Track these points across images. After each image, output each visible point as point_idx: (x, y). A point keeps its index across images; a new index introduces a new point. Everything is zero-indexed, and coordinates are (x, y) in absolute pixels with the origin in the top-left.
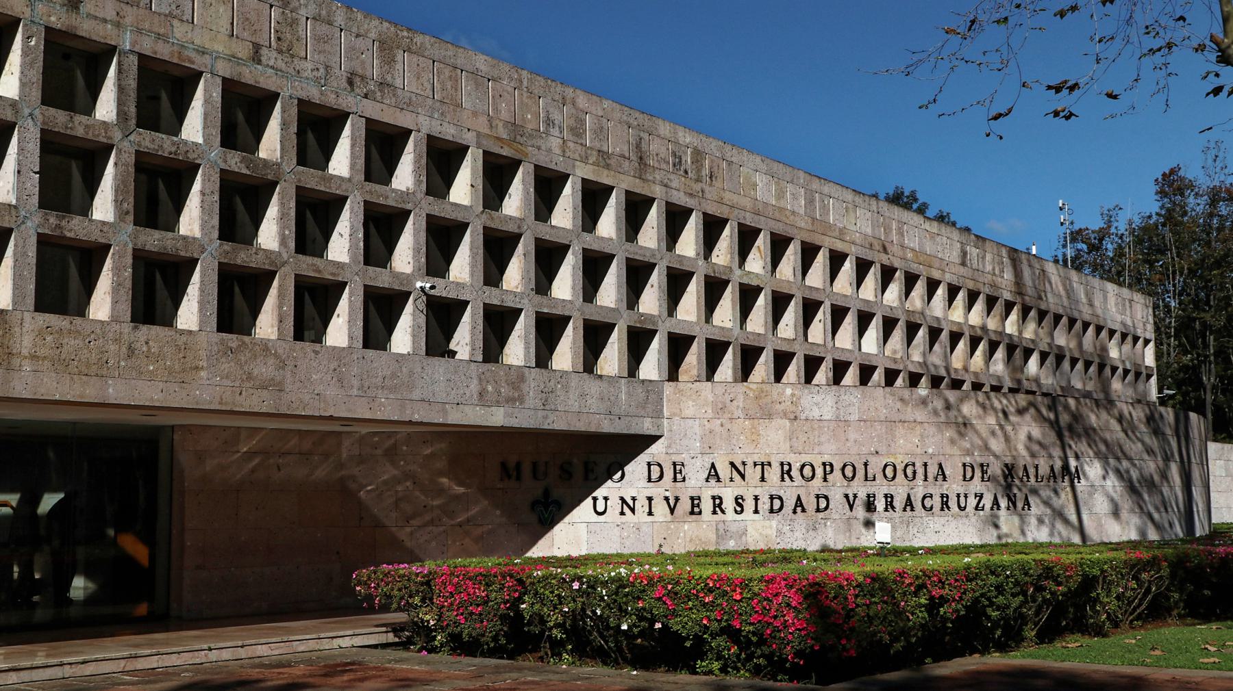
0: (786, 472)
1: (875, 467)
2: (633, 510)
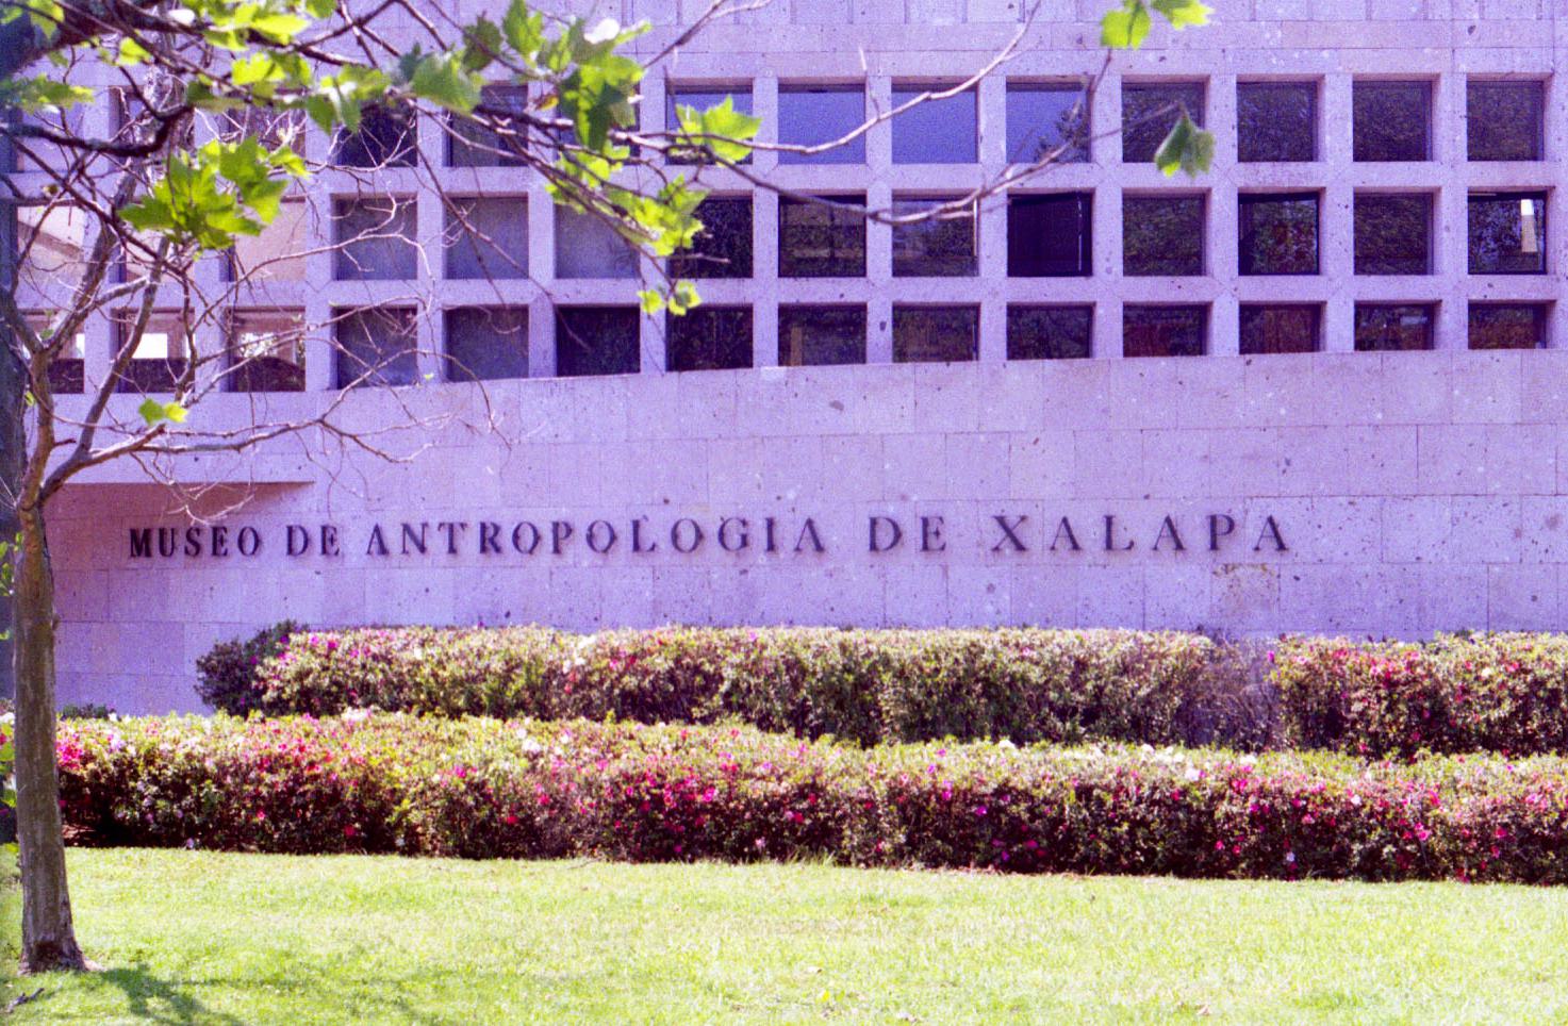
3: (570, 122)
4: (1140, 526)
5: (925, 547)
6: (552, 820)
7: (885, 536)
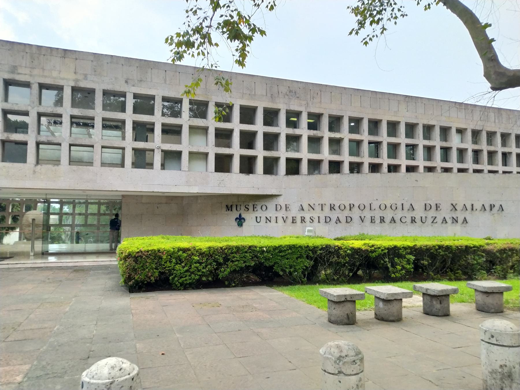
0: (332, 208)
1: (375, 206)
2: (270, 221)
3: (295, 119)
4: (478, 206)
5: (437, 210)
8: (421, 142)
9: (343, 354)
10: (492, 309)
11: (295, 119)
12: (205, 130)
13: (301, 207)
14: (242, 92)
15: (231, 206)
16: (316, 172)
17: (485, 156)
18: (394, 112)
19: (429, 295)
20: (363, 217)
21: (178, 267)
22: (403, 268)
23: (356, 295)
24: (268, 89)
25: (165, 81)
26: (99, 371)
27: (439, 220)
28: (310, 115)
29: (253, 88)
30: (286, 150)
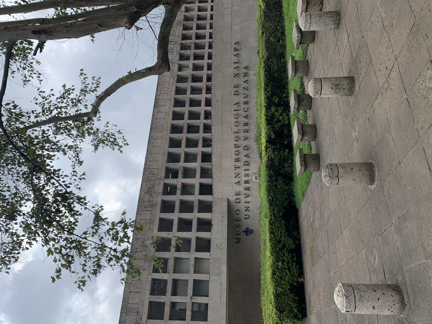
0: (237, 160)
1: (235, 129)
2: (248, 207)
3: (169, 187)
4: (235, 59)
5: (238, 87)
6: (46, 194)
7: (237, 93)
8: (188, 96)
9: (328, 175)
10: (306, 68)
11: (169, 187)
12: (176, 259)
13: (237, 184)
14: (148, 230)
15: (236, 239)
16: (210, 171)
17: (198, 51)
18: (166, 115)
19: (298, 107)
20: (244, 138)
21: (287, 279)
22: (281, 115)
23: (300, 154)
24: (146, 209)
25: (138, 292)
26: (340, 303)
27: (245, 85)
28: (167, 177)
29: (145, 221)
30: (193, 195)
